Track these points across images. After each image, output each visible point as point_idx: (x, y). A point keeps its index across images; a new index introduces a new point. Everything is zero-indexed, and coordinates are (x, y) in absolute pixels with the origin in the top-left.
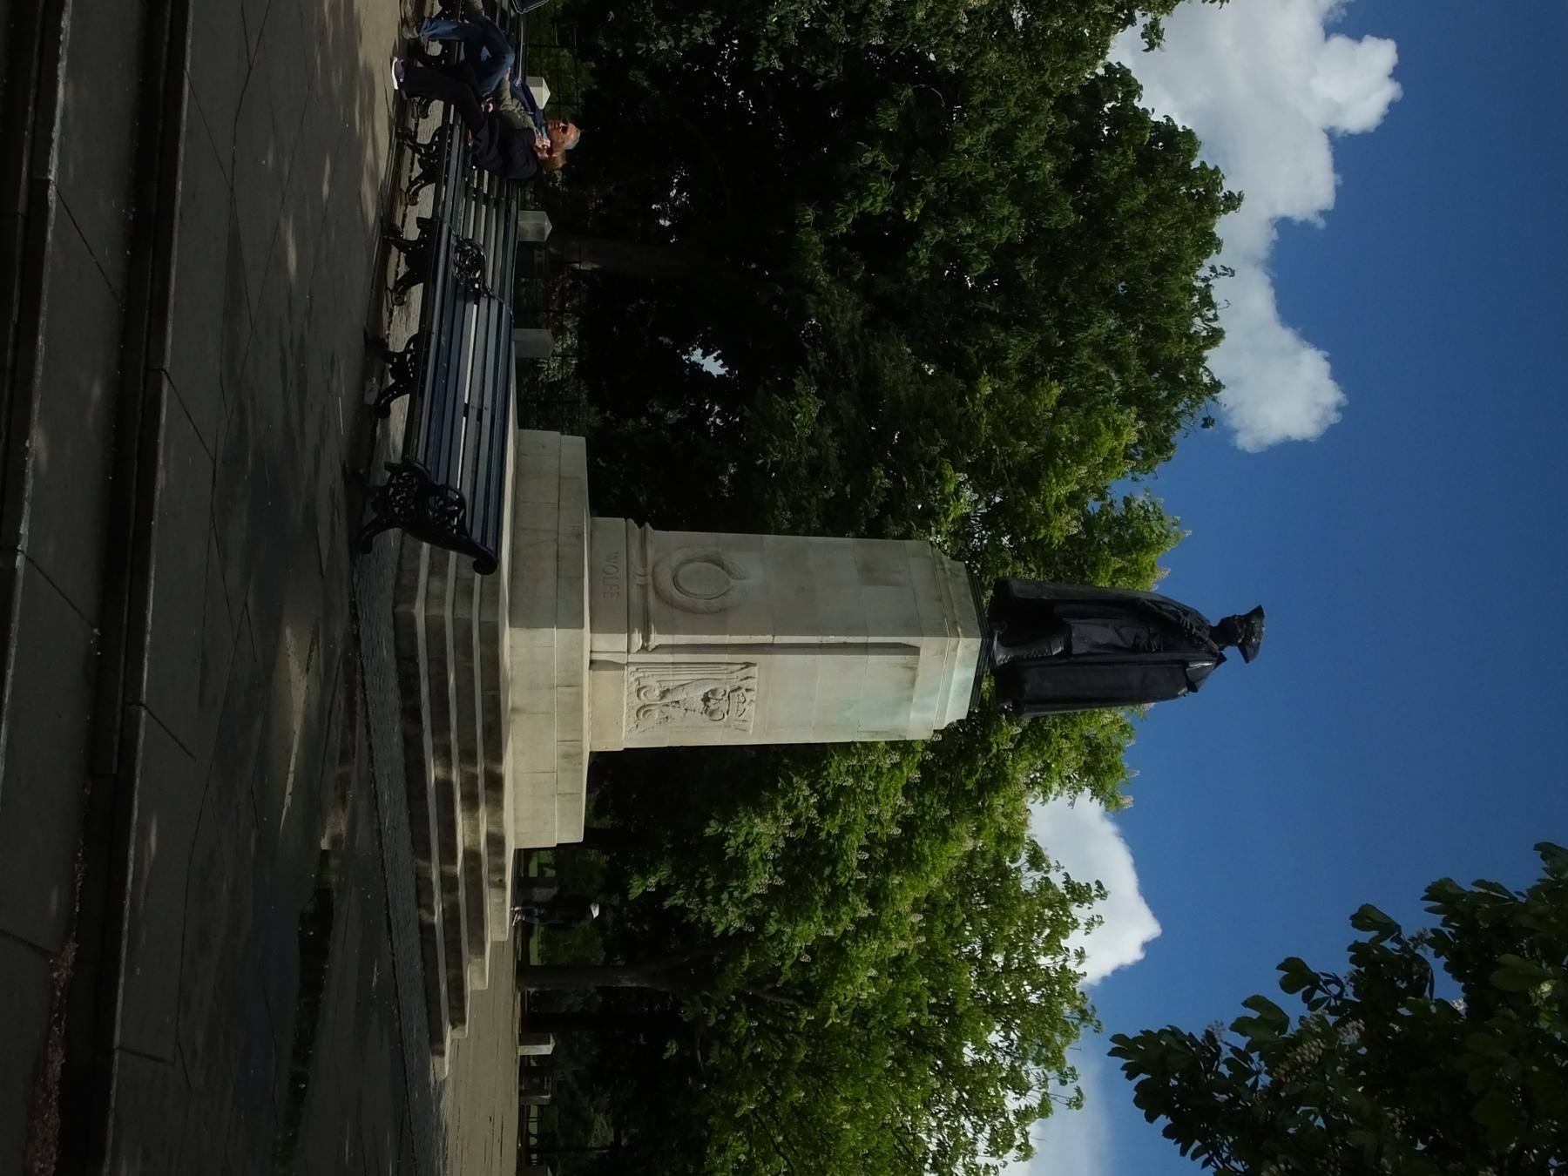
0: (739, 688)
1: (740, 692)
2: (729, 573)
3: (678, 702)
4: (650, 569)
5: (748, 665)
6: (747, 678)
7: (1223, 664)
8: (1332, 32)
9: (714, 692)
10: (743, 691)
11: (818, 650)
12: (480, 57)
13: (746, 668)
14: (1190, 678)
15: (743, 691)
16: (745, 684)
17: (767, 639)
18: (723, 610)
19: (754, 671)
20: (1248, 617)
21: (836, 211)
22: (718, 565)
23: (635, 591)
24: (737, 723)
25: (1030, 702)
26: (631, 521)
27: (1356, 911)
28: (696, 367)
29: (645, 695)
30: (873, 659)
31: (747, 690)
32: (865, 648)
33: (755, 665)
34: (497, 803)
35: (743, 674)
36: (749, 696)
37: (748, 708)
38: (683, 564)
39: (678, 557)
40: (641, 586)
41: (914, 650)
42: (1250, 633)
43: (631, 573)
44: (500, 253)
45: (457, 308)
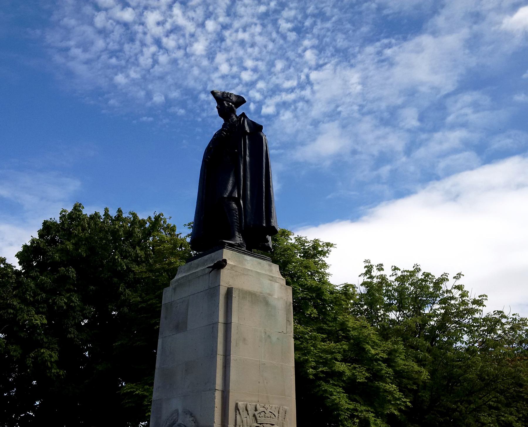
0: (254, 415)
1: (257, 416)
5: (237, 408)
6: (247, 410)
8: (294, 31)
10: (256, 413)
11: (228, 357)
12: (261, 112)
13: (239, 410)
15: (256, 413)
16: (251, 412)
17: (218, 396)
19: (241, 404)
24: (280, 419)
27: (21, 249)
28: (35, 381)
30: (235, 319)
31: (256, 410)
32: (228, 325)
33: (237, 405)
35: (244, 414)
36: (260, 409)
37: (269, 410)
41: (229, 292)
42: (205, 15)
45: (265, 148)
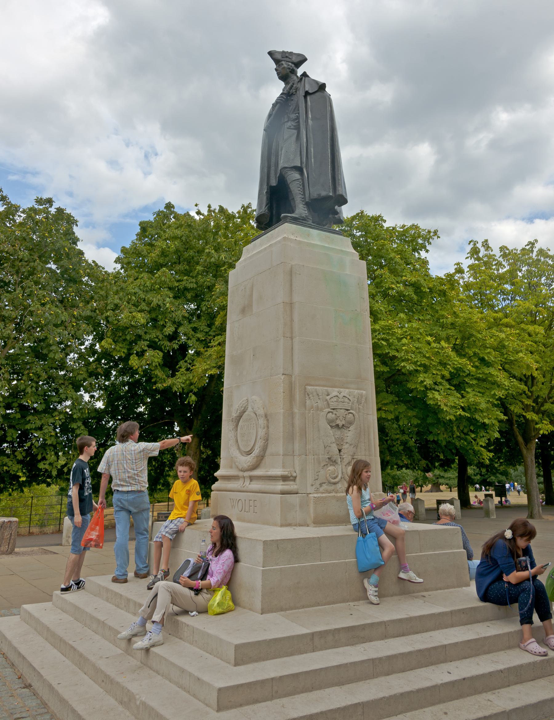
2: (244, 412)
3: (340, 451)
4: (241, 474)
7: (308, 74)
9: (330, 422)
14: (316, 90)
15: (328, 398)
18: (266, 416)
20: (277, 62)
21: (491, 456)
22: (240, 419)
23: (255, 486)
25: (335, 189)
26: (214, 487)
29: (335, 478)
34: (356, 246)
38: (239, 448)
39: (235, 453)
40: (251, 481)
43: (244, 489)
44: (372, 442)
